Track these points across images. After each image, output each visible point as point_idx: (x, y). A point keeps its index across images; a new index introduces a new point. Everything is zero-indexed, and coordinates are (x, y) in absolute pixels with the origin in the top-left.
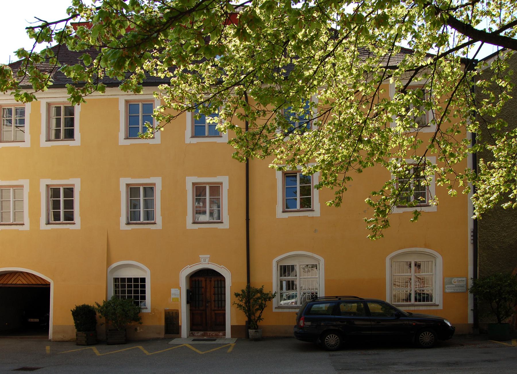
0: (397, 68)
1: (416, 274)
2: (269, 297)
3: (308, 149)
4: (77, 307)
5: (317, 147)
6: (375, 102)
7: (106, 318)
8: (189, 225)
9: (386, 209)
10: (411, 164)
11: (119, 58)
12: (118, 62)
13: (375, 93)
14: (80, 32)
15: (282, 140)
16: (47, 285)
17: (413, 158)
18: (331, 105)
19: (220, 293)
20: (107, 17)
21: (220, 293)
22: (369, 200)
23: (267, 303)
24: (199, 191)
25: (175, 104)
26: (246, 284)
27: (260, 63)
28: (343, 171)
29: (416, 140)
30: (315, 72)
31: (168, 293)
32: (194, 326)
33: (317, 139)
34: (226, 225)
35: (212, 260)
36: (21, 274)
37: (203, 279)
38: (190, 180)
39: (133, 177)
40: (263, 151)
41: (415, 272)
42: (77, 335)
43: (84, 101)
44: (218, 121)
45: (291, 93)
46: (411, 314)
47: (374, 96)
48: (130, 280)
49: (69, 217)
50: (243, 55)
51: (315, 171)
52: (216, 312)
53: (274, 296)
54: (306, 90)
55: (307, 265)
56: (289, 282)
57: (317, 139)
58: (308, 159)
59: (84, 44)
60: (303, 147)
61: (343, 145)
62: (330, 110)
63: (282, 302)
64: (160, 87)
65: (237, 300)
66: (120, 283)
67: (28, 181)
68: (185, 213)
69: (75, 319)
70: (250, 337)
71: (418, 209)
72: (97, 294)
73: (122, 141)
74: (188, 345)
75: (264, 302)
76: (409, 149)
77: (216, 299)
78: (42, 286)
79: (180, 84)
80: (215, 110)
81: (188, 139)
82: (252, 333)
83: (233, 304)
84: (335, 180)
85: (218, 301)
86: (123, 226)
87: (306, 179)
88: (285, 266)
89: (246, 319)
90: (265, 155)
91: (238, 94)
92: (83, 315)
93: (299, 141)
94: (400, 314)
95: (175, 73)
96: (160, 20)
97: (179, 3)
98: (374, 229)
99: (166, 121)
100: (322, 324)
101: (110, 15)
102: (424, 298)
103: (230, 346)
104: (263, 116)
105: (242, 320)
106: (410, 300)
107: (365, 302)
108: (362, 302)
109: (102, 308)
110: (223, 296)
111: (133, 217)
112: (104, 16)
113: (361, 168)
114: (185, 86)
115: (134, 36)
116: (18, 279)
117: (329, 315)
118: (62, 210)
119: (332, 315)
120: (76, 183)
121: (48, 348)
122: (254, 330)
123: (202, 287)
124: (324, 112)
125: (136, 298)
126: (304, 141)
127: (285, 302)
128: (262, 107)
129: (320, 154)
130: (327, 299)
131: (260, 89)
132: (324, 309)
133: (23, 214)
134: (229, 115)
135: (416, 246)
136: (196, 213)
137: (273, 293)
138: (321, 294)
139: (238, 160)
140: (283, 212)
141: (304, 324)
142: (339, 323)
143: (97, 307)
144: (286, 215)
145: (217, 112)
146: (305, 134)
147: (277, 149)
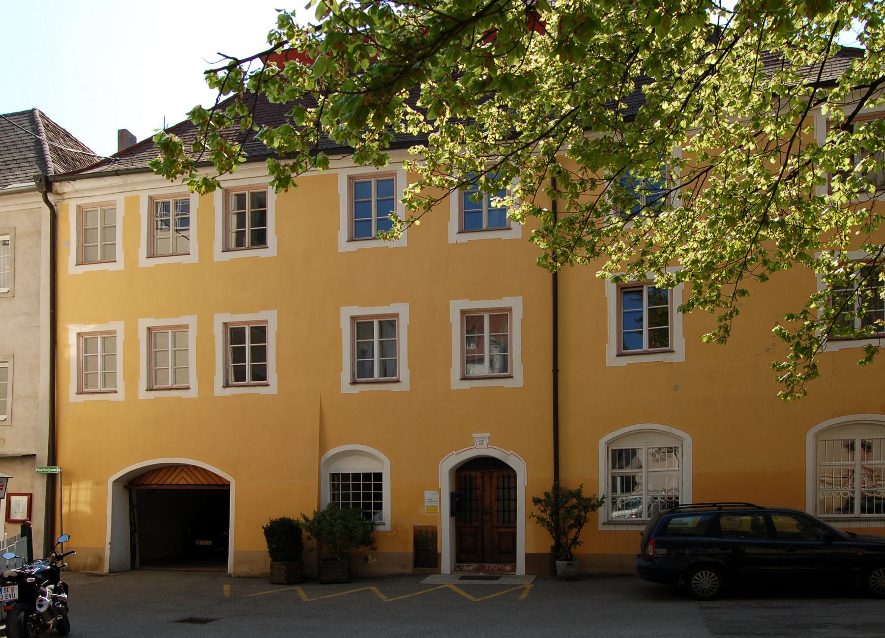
0: (837, 85)
1: (864, 463)
2: (591, 505)
3: (668, 242)
4: (272, 522)
5: (684, 237)
6: (794, 150)
7: (318, 540)
8: (456, 383)
9: (812, 344)
10: (862, 261)
11: (358, 109)
12: (358, 115)
13: (794, 135)
14: (290, 72)
15: (621, 228)
16: (224, 485)
17: (865, 249)
18: (712, 161)
19: (506, 497)
20: (341, 43)
21: (506, 497)
22: (781, 329)
23: (589, 515)
24: (472, 323)
25: (439, 178)
26: (552, 483)
27: (586, 97)
28: (734, 279)
29: (870, 215)
30: (685, 105)
31: (419, 500)
32: (462, 554)
33: (684, 223)
34: (518, 379)
35: (493, 442)
36: (185, 469)
37: (479, 474)
38: (457, 307)
39: (362, 305)
40: (587, 249)
41: (863, 460)
42: (272, 568)
43: (295, 185)
44: (512, 201)
45: (641, 146)
46: (853, 536)
47: (792, 141)
48: (356, 476)
49: (260, 375)
50: (553, 84)
51: (679, 281)
52: (500, 530)
53: (601, 503)
54: (668, 139)
55: (660, 449)
56: (627, 477)
57: (684, 223)
58: (667, 259)
59: (295, 90)
60: (658, 238)
61: (733, 233)
62: (707, 171)
63: (615, 514)
64: (411, 150)
65: (536, 510)
66: (340, 481)
67: (274, 313)
68: (448, 364)
69: (269, 541)
70: (559, 573)
71: (874, 343)
72: (304, 501)
73: (344, 245)
74: (452, 587)
75: (583, 513)
76: (857, 233)
77: (501, 509)
78: (217, 488)
79: (444, 142)
80: (506, 183)
81: (453, 235)
82: (562, 566)
83: (530, 516)
84: (718, 296)
85: (504, 511)
86: (346, 387)
87: (659, 297)
88: (621, 451)
89: (552, 542)
90: (590, 257)
91: (545, 153)
92: (282, 535)
93: (650, 228)
94: (832, 536)
95: (436, 124)
96: (423, 39)
97: (454, 6)
98: (790, 382)
99: (424, 208)
100: (687, 552)
101: (344, 39)
102: (878, 505)
103: (524, 588)
104: (591, 189)
105: (545, 543)
106: (852, 511)
107: (767, 513)
108: (760, 514)
109: (312, 523)
110: (512, 502)
111: (362, 372)
112: (336, 40)
113: (767, 273)
114: (454, 146)
115: (382, 69)
116: (180, 476)
117: (700, 536)
118: (248, 364)
119: (704, 536)
120: (271, 319)
121: (226, 587)
122: (566, 562)
123: (477, 489)
124: (697, 174)
125: (367, 506)
126: (659, 227)
127: (620, 512)
128: (590, 174)
129: (687, 251)
130: (696, 509)
131: (586, 142)
132: (690, 525)
133: (188, 372)
134: (529, 191)
135: (864, 411)
136: (468, 362)
137: (600, 497)
138: (686, 499)
139: (547, 268)
140: (618, 356)
141: (654, 552)
142: (718, 550)
143: (304, 521)
144: (624, 361)
145: (508, 187)
146: (662, 216)
147: (611, 244)
